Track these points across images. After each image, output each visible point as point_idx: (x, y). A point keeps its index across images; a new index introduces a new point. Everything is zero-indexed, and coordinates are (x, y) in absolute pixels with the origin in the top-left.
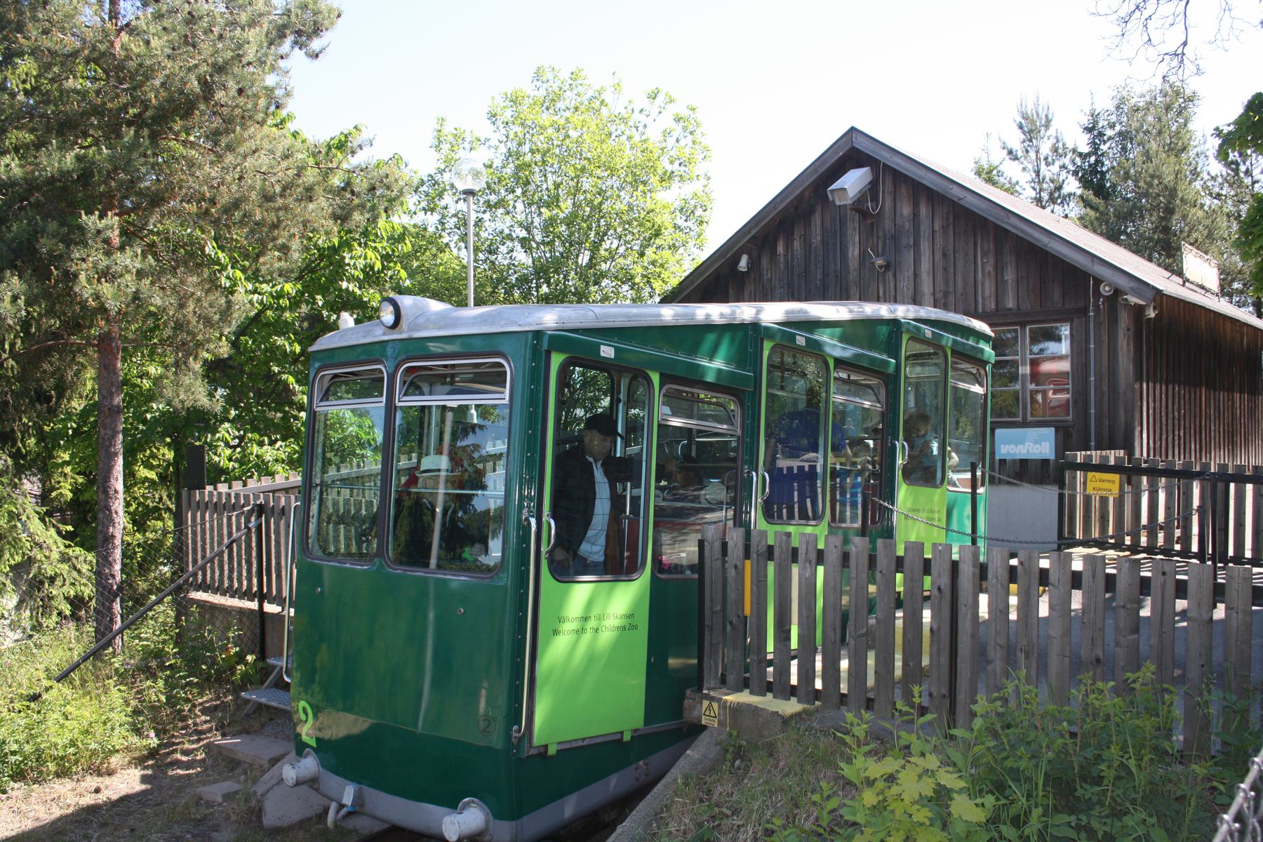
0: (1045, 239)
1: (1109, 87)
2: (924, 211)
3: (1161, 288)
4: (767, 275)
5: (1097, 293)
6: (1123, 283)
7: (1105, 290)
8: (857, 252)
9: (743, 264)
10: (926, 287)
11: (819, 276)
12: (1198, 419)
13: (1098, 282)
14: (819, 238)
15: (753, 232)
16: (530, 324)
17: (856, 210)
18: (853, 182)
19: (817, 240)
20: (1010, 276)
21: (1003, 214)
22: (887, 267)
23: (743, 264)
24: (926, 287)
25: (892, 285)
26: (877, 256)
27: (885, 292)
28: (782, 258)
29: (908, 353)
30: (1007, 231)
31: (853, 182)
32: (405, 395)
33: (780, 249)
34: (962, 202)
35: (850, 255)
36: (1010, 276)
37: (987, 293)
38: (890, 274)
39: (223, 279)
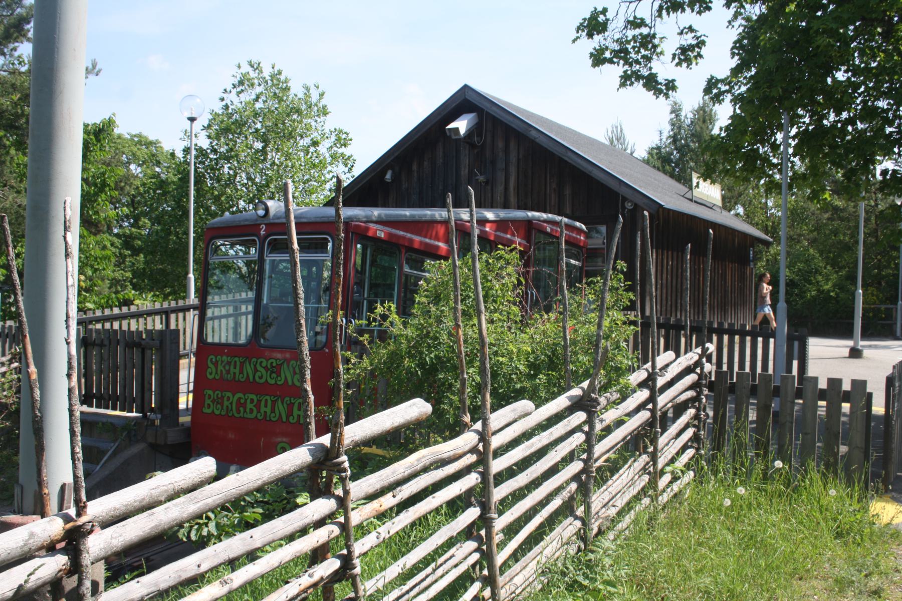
0: (590, 168)
1: (728, 27)
2: (513, 145)
3: (663, 204)
4: (405, 186)
5: (624, 208)
6: (640, 201)
7: (629, 206)
8: (467, 171)
9: (388, 176)
10: (513, 199)
11: (441, 188)
12: (697, 293)
13: (625, 199)
14: (441, 161)
15: (396, 154)
16: (175, 505)
17: (468, 143)
18: (462, 125)
19: (440, 161)
20: (568, 192)
21: (564, 150)
22: (487, 183)
23: (388, 176)
24: (513, 199)
25: (490, 195)
26: (481, 175)
27: (485, 199)
28: (415, 174)
29: (536, 241)
30: (566, 162)
31: (462, 125)
32: (270, 253)
33: (415, 167)
34: (537, 140)
35: (462, 173)
36: (568, 192)
37: (553, 203)
38: (489, 188)
39: (111, 212)
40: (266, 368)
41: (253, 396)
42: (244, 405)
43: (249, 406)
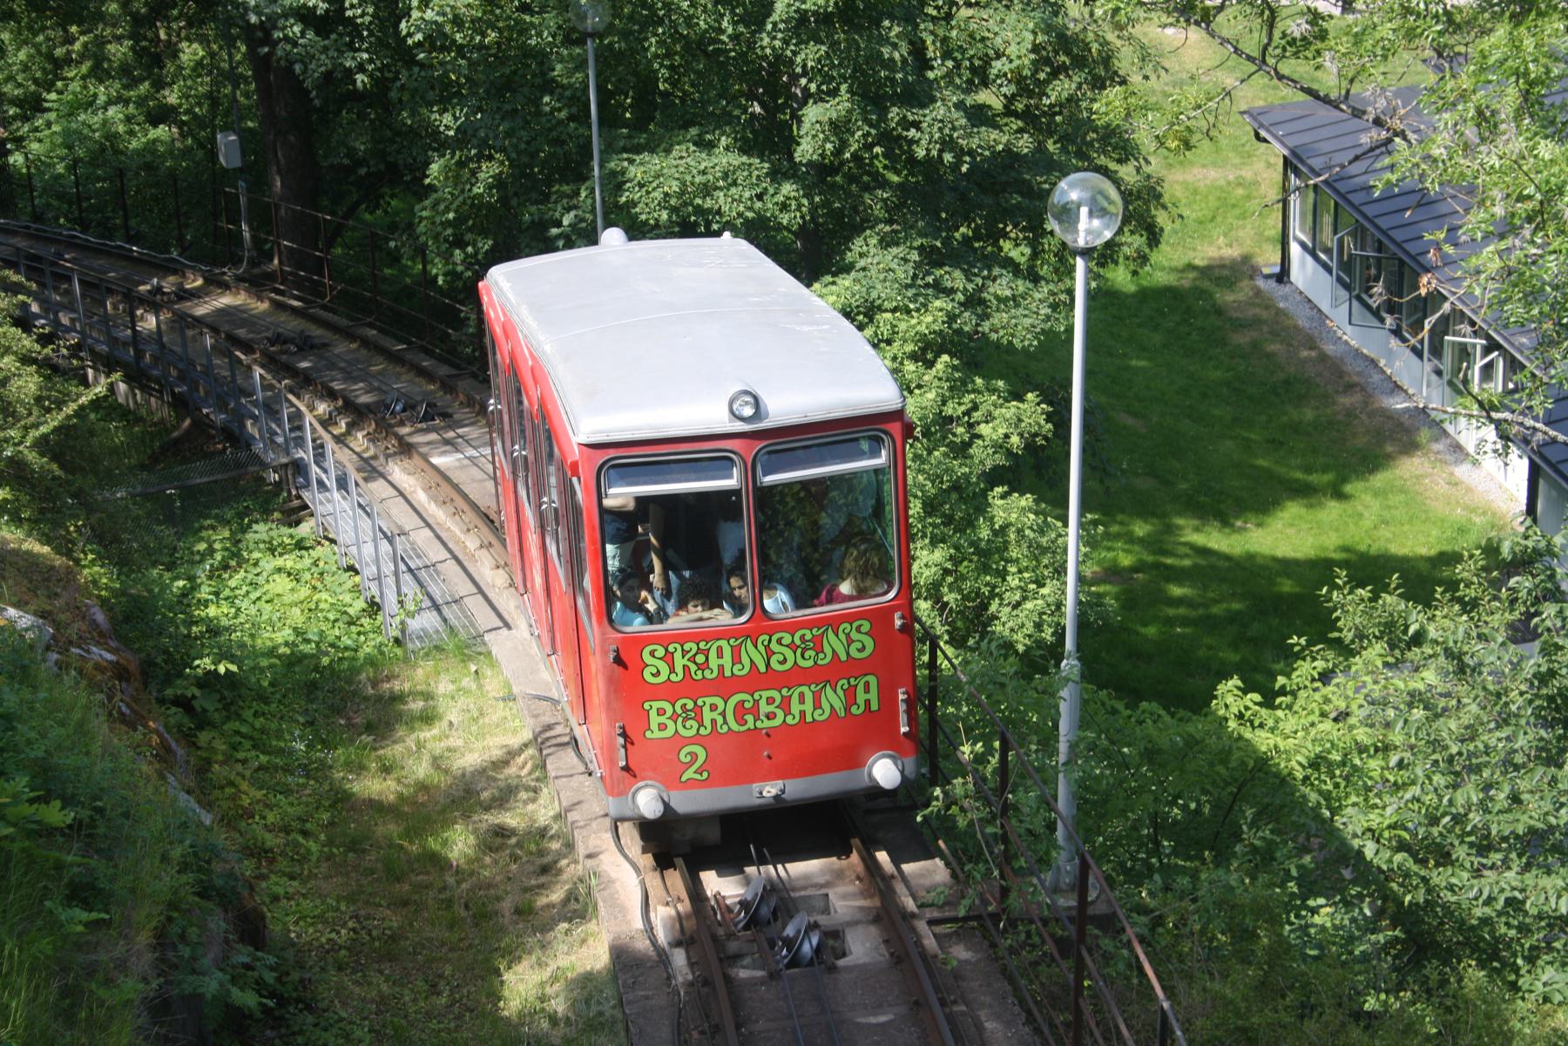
40: (793, 647)
41: (774, 693)
42: (755, 711)
43: (764, 708)
